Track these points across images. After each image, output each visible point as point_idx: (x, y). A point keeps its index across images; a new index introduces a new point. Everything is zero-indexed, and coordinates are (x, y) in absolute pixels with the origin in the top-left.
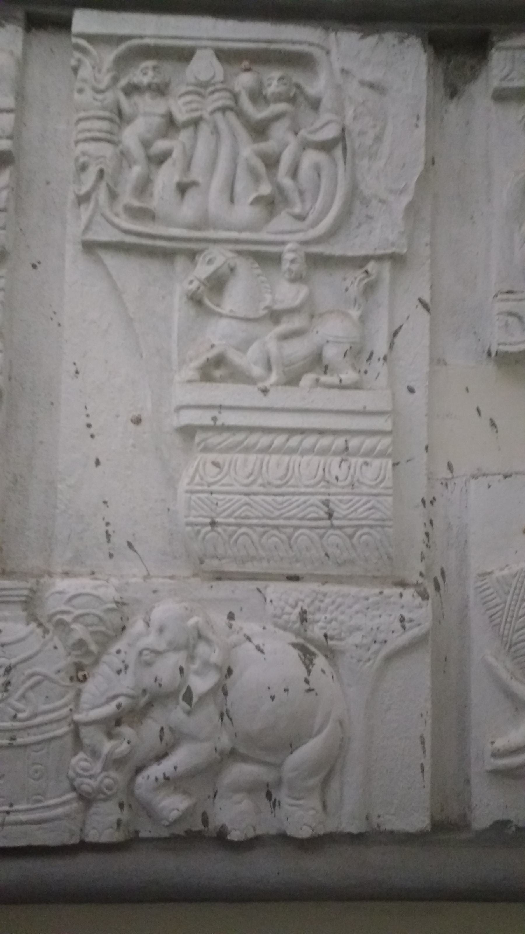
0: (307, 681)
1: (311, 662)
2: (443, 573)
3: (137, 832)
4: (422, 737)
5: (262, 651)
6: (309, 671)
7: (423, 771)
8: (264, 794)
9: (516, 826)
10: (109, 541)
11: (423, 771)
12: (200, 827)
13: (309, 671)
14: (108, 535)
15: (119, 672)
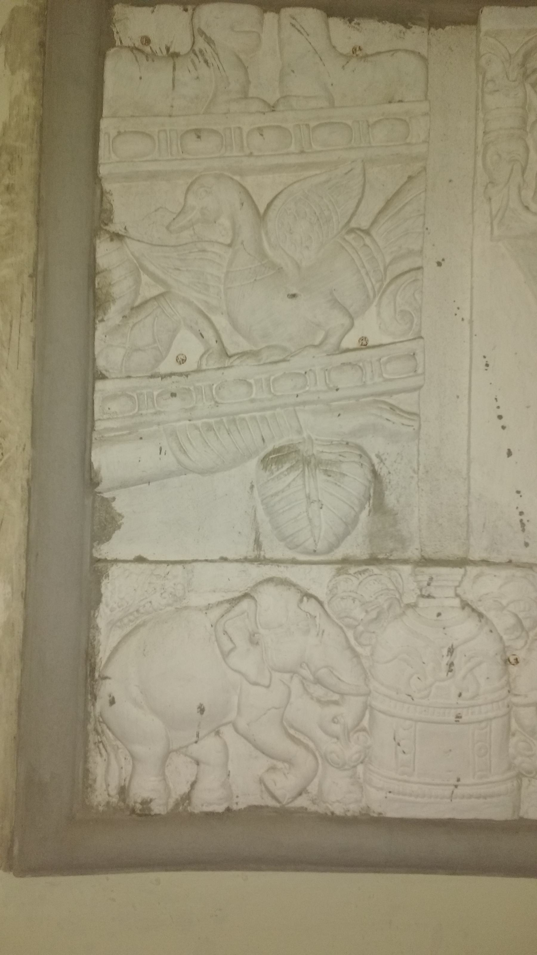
10: (523, 530)
14: (523, 525)
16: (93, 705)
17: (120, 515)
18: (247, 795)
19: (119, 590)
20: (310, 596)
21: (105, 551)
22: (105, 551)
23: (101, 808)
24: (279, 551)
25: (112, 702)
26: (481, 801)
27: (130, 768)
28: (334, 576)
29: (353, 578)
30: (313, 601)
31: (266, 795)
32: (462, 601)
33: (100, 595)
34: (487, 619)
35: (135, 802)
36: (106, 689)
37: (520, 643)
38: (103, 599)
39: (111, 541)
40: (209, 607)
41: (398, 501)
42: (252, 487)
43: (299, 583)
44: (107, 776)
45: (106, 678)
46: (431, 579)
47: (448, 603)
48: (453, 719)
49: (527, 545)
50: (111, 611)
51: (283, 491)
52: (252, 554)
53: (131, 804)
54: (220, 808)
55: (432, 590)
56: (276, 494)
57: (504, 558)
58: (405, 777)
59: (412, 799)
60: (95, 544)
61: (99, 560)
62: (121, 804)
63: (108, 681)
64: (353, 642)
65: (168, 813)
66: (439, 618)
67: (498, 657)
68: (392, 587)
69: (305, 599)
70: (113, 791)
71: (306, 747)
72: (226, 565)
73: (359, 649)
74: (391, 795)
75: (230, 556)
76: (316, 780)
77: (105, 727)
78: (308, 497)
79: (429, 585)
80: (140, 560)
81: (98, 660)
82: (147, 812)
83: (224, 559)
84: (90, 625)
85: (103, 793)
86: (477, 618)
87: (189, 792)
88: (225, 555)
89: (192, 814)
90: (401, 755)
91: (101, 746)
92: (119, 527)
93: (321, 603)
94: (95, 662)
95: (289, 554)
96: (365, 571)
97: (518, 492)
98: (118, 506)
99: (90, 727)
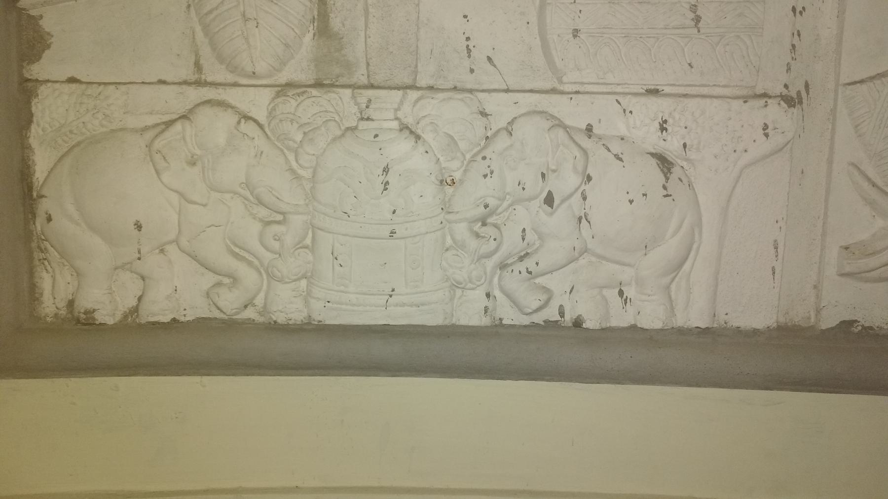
0: (665, 188)
1: (669, 170)
2: (807, 86)
3: (501, 319)
4: (775, 241)
5: (621, 160)
6: (667, 179)
7: (774, 273)
8: (617, 290)
9: (863, 326)
10: (469, 56)
11: (774, 273)
12: (558, 318)
13: (667, 179)
14: (469, 50)
15: (485, 176)
16: (34, 224)
17: (49, 34)
18: (194, 307)
19: (52, 110)
20: (247, 118)
21: (36, 71)
22: (36, 71)
23: (48, 319)
24: (220, 74)
25: (49, 219)
26: (415, 308)
27: (76, 283)
28: (274, 99)
29: (292, 101)
30: (251, 123)
31: (214, 308)
32: (401, 123)
33: (32, 115)
34: (424, 141)
35: (79, 313)
36: (44, 206)
37: (455, 164)
38: (35, 119)
39: (42, 61)
40: (146, 129)
41: (343, 25)
42: (189, 6)
43: (238, 105)
44: (54, 291)
45: (43, 196)
46: (370, 101)
47: (387, 125)
48: (388, 234)
49: (472, 71)
50: (43, 130)
51: (216, 8)
52: (193, 78)
53: (76, 314)
54: (166, 319)
55: (370, 112)
56: (210, 12)
57: (450, 85)
58: (342, 288)
59: (349, 307)
60: (25, 64)
61: (28, 80)
62: (70, 316)
63: (44, 199)
64: (294, 164)
65: (115, 324)
66: (376, 139)
67: (433, 178)
68: (332, 109)
69: (243, 121)
70: (62, 304)
71: (250, 263)
72: (163, 87)
73: (301, 172)
74: (330, 304)
75: (169, 79)
76: (262, 295)
77: (49, 246)
78: (244, 15)
79: (367, 107)
80: (72, 80)
81: (34, 180)
82: (91, 321)
83: (162, 82)
84: (24, 147)
85: (51, 304)
86: (414, 140)
87: (138, 306)
88: (163, 78)
89: (140, 325)
90: (337, 268)
91: (46, 263)
92: (49, 47)
93: (261, 126)
94: (32, 182)
95: (230, 78)
96: (304, 92)
97: (465, 17)
98: (47, 24)
99: (34, 245)
